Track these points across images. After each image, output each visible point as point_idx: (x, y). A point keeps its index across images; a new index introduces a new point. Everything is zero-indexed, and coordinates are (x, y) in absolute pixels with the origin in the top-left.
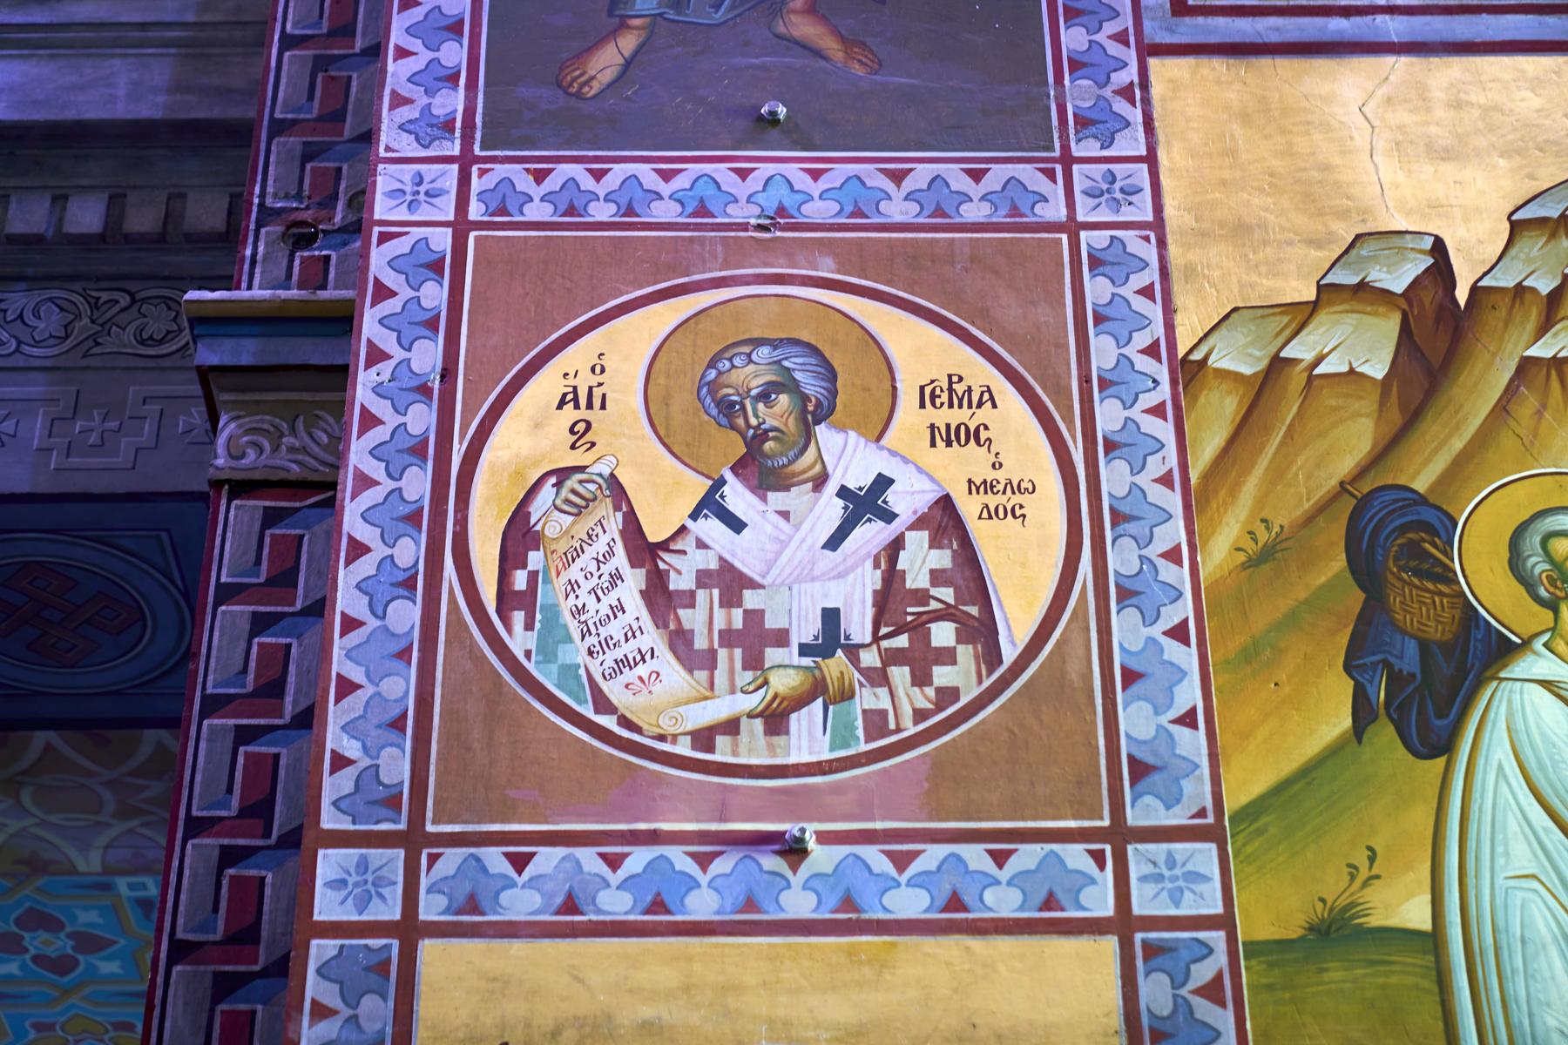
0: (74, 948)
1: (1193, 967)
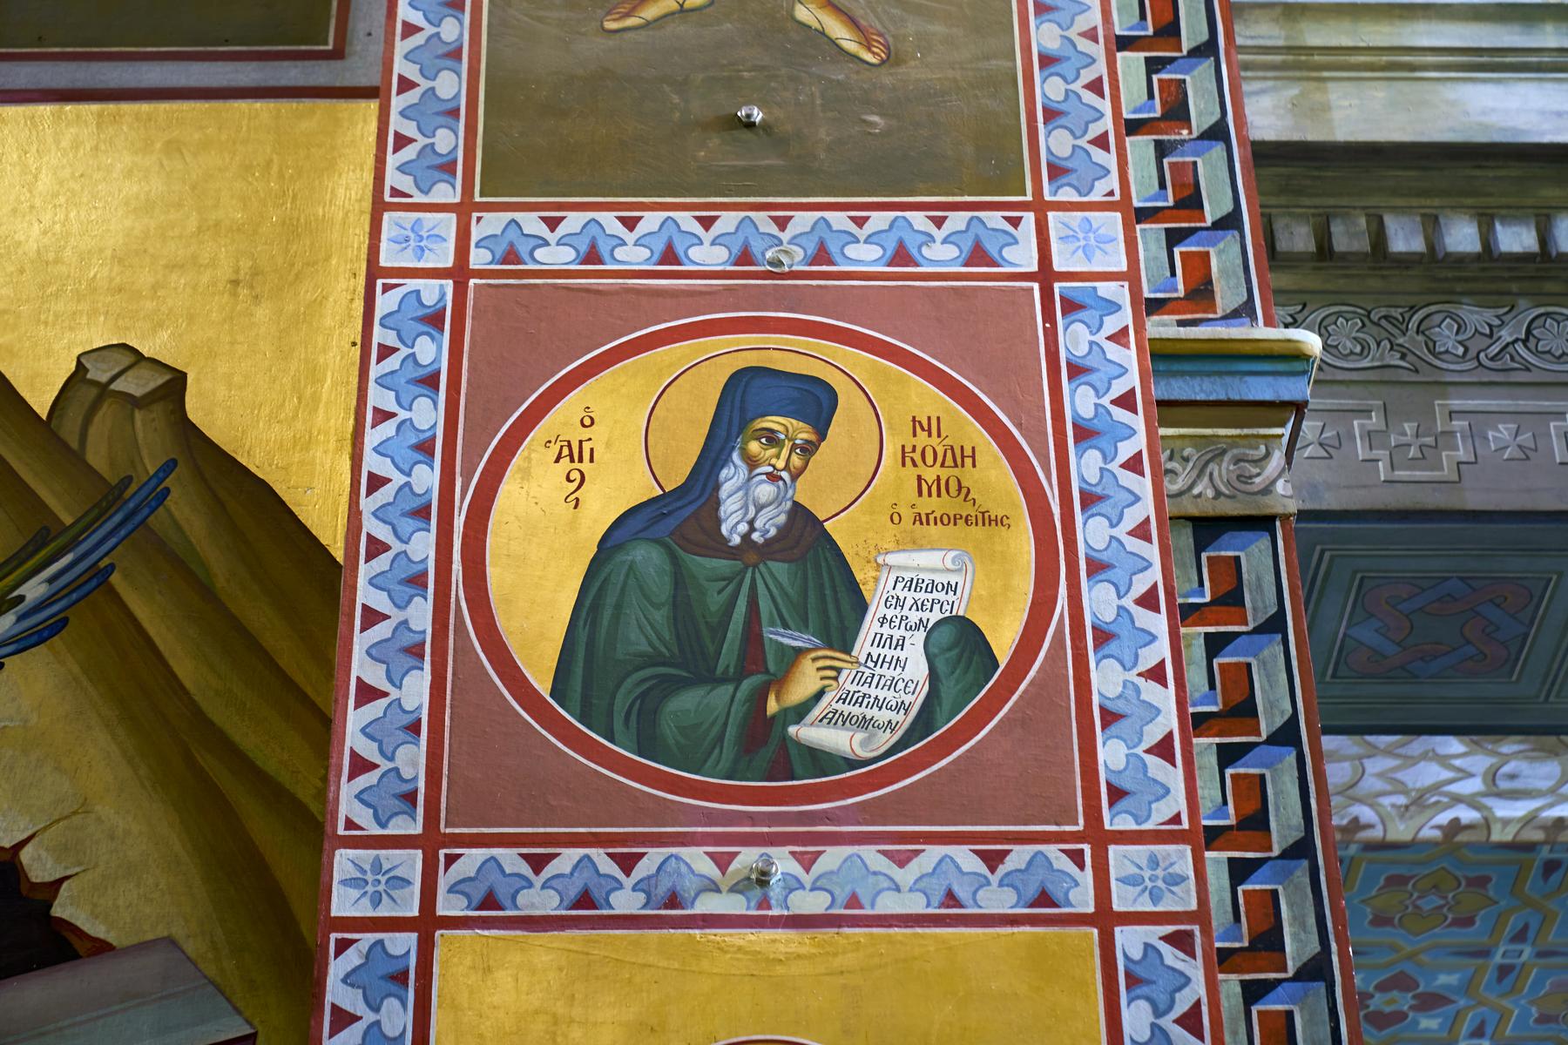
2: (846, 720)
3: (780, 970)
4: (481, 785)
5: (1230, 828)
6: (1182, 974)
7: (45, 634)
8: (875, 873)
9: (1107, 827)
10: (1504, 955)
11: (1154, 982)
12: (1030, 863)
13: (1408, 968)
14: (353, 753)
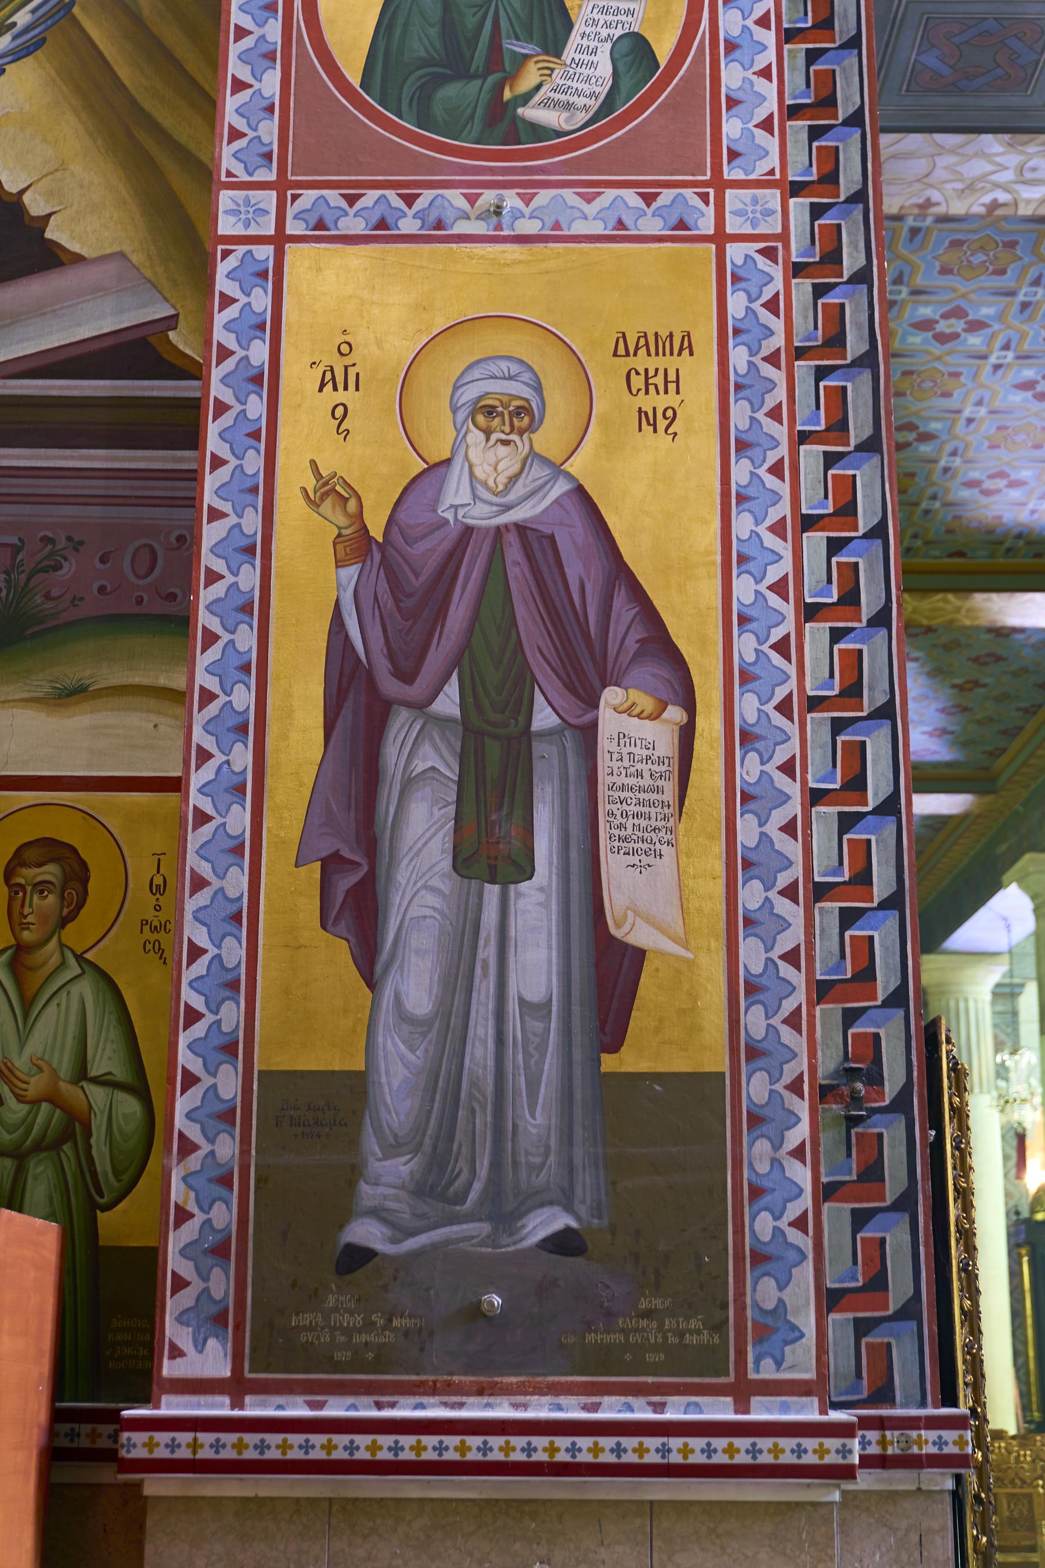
2: (556, 104)
3: (508, 270)
4: (316, 149)
5: (813, 182)
6: (768, 274)
7: (32, 49)
8: (572, 207)
9: (726, 177)
10: (1025, 295)
11: (749, 280)
12: (673, 201)
13: (963, 304)
14: (230, 126)
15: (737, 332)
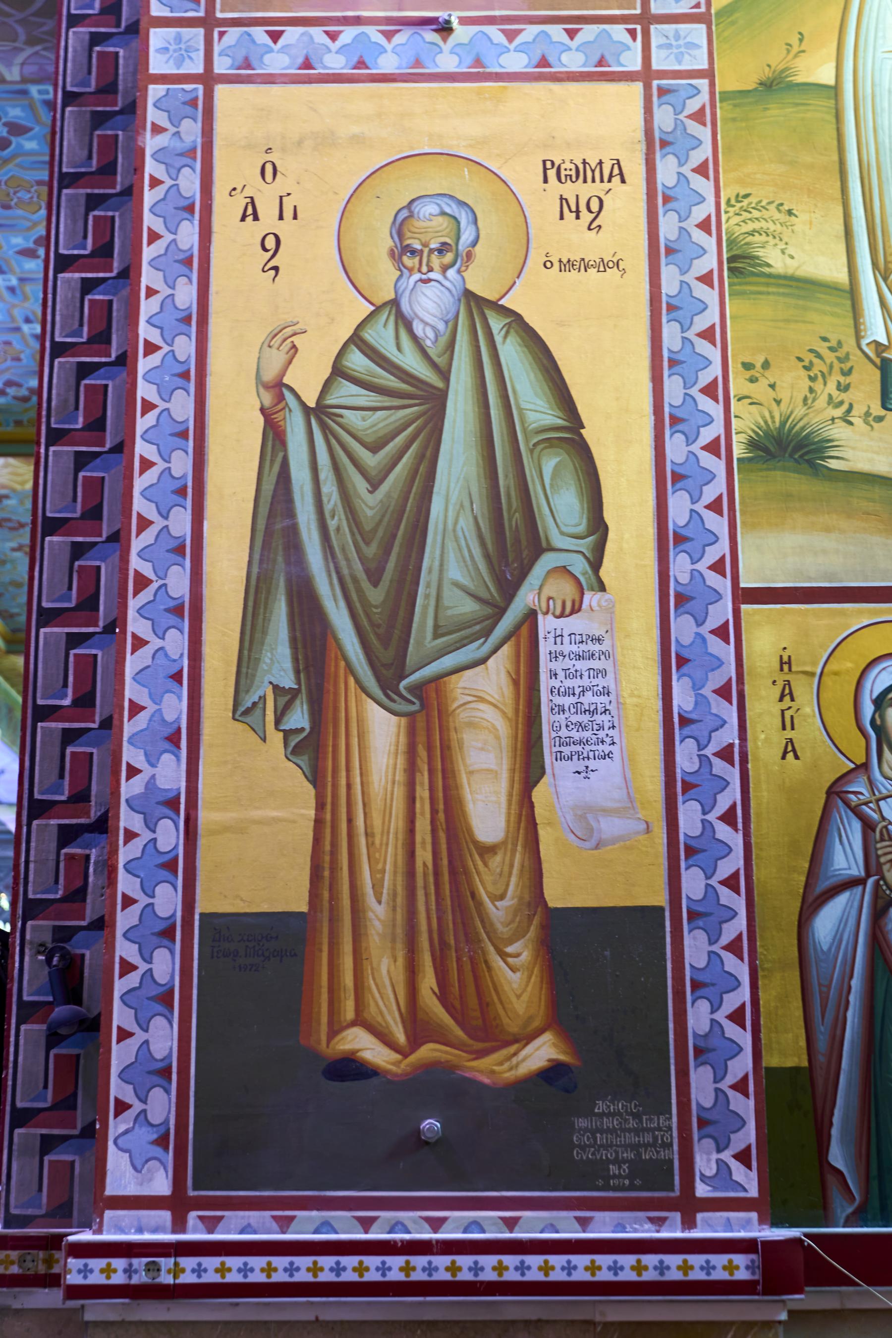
0: (8, 132)
1: (687, 101)
15: (670, 251)
